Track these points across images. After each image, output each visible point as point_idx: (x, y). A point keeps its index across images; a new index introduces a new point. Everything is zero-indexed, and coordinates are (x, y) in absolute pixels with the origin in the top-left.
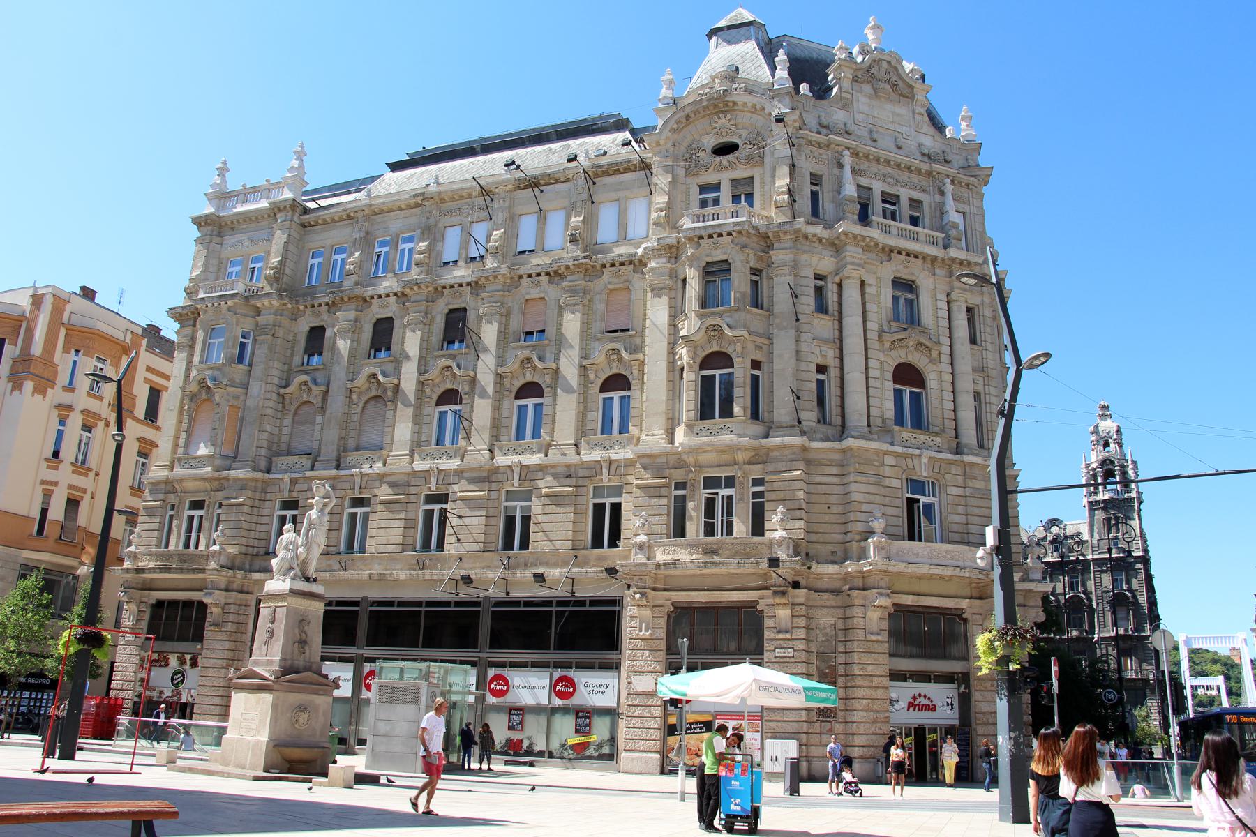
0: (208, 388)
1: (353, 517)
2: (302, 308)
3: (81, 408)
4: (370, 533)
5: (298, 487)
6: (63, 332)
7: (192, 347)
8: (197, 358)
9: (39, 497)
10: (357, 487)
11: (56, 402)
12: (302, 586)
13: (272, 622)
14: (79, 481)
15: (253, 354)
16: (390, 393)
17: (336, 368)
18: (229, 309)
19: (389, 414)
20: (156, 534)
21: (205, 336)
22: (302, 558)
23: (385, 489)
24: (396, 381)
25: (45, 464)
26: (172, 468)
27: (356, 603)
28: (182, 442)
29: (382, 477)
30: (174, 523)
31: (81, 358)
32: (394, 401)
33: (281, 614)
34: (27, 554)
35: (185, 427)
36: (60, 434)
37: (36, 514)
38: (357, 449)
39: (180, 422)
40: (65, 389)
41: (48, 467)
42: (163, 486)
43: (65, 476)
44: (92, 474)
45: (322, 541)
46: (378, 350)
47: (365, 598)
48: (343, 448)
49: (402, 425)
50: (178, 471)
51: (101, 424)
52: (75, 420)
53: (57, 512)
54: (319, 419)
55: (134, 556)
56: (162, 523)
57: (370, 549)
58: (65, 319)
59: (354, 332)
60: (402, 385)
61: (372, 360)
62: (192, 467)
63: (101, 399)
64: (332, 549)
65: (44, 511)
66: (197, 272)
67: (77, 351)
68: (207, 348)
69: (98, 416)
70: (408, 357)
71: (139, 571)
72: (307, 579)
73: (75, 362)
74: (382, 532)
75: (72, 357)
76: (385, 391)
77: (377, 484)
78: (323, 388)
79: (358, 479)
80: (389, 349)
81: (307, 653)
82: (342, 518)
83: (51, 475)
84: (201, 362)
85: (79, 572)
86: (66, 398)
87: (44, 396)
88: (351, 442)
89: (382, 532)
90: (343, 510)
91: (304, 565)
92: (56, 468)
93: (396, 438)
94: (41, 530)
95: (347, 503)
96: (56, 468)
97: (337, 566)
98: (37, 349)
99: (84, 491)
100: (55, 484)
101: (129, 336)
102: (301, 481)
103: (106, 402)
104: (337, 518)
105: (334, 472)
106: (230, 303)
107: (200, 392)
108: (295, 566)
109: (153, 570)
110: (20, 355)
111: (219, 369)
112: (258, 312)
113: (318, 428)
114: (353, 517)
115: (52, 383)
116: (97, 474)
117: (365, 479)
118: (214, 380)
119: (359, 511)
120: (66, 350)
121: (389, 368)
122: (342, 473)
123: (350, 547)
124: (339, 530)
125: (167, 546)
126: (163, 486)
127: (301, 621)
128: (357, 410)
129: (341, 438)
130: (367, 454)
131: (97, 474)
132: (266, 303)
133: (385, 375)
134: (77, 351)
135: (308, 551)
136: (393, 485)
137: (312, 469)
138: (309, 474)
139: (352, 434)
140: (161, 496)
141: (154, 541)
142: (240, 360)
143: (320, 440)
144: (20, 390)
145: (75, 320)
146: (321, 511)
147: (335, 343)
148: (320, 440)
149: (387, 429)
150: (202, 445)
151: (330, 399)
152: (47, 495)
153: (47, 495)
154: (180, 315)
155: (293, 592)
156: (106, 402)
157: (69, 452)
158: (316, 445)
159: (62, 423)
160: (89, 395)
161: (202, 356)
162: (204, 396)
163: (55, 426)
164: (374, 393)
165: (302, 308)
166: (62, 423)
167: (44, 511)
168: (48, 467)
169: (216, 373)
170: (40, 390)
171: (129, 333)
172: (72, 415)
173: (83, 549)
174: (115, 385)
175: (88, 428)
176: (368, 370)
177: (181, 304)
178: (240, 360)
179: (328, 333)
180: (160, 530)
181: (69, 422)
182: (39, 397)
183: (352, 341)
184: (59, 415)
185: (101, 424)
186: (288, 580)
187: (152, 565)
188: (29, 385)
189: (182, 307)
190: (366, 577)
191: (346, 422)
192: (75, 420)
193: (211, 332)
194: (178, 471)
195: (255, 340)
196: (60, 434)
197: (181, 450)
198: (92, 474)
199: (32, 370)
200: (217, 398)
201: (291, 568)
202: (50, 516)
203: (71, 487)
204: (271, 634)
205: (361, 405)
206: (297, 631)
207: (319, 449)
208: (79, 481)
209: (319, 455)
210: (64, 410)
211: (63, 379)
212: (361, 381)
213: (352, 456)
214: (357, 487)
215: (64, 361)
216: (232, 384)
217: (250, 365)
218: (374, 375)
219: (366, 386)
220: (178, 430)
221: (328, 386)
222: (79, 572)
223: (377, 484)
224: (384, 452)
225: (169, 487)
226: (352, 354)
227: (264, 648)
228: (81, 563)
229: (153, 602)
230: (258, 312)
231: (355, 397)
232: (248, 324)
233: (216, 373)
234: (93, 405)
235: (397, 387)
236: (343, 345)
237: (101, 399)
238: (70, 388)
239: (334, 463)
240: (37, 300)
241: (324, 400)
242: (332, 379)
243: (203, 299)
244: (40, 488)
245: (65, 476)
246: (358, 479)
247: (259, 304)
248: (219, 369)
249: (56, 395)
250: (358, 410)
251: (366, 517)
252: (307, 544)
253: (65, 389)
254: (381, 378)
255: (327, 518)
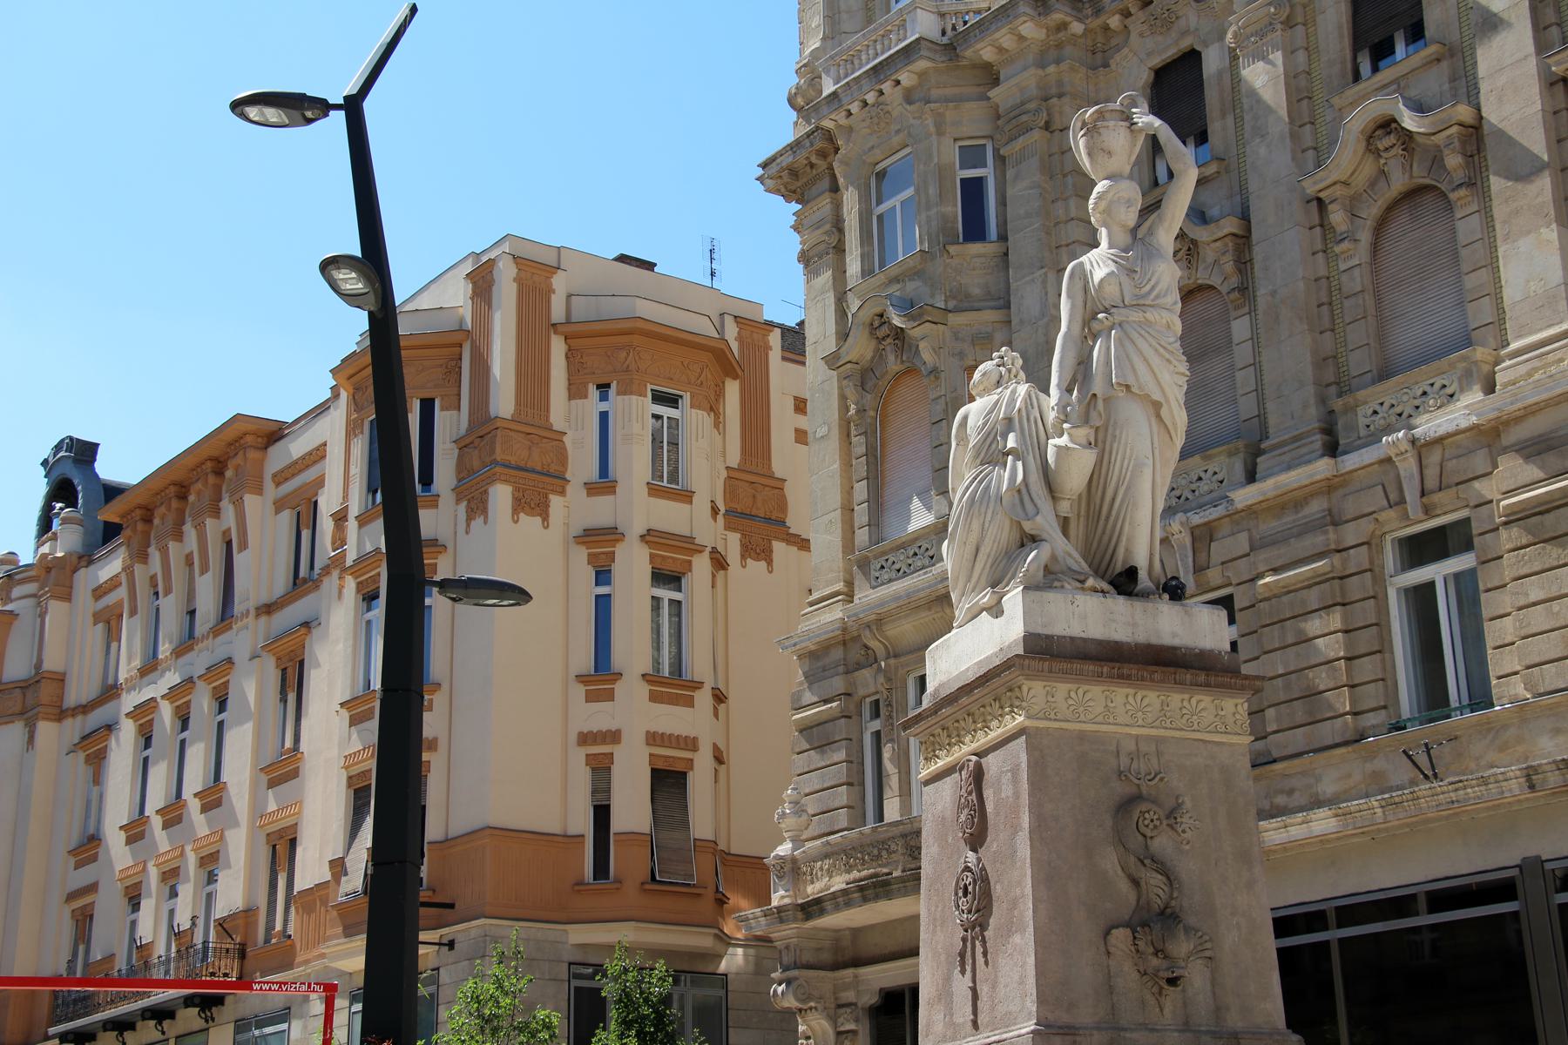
0: (899, 334)
1: (1422, 598)
2: (1115, 22)
3: (639, 528)
4: (1494, 632)
5: (1219, 550)
6: (558, 347)
7: (840, 249)
8: (853, 266)
9: (582, 778)
10: (1411, 494)
11: (577, 529)
12: (1091, 615)
13: (976, 840)
14: (672, 720)
15: (1002, 202)
16: (1453, 161)
17: (1259, 151)
18: (909, 98)
19: (1468, 227)
20: (842, 795)
21: (865, 199)
22: (1075, 479)
23: (1512, 469)
24: (1464, 112)
25: (580, 690)
26: (850, 596)
27: (1502, 889)
28: (861, 514)
29: (1489, 438)
30: (887, 753)
31: (617, 403)
32: (1475, 182)
33: (1008, 778)
34: (580, 935)
35: (860, 466)
36: (603, 606)
37: (582, 823)
38: (1384, 373)
39: (847, 464)
40: (592, 489)
41: (591, 697)
42: (837, 654)
43: (635, 713)
44: (704, 698)
45: (1169, 378)
46: (1382, 52)
47: (1532, 865)
48: (1335, 383)
49: (1524, 244)
50: (868, 596)
51: (701, 566)
52: (633, 564)
53: (633, 810)
54: (1240, 328)
55: (794, 870)
56: (855, 762)
57: (1509, 691)
58: (558, 312)
59: (1289, 24)
60: (1491, 114)
61: (1370, 82)
62: (901, 574)
63: (686, 496)
64: (1371, 720)
65: (602, 814)
66: (815, 44)
67: (603, 388)
68: (875, 231)
69: (688, 545)
70: (1491, 23)
71: (812, 909)
72: (1125, 582)
73: (604, 417)
74: (1538, 619)
75: (592, 404)
76: (1436, 160)
77: (1480, 462)
78: (1230, 225)
79: (1407, 467)
80: (1416, 33)
81: (1197, 977)
82: (1383, 610)
83: (599, 717)
84: (867, 272)
85: (723, 967)
86: (600, 511)
87: (545, 518)
88: (1359, 362)
89: (1538, 619)
90: (1380, 581)
91: (1095, 515)
92: (609, 696)
93: (1510, 294)
94: (601, 868)
95: (1390, 558)
96: (609, 696)
97: (1404, 772)
98: (503, 403)
99: (691, 744)
100: (614, 737)
101: (731, 331)
102: (1226, 527)
103: (701, 504)
104: (1367, 612)
105: (1323, 467)
106: (906, 78)
107: (879, 355)
108: (1045, 522)
109: (843, 899)
110: (470, 430)
111: (916, 274)
112: (991, 76)
113: (1243, 354)
114: (1422, 598)
115: (558, 480)
116: (719, 697)
117: (1434, 458)
118: (908, 306)
119: (1436, 572)
120: (575, 391)
121: (1433, 83)
122: (1351, 461)
123: (1434, 699)
124: (1383, 648)
125: (880, 816)
126: (837, 654)
127: (1126, 805)
128: (1355, 254)
129: (1321, 362)
130: (1420, 379)
131: (719, 697)
132: (1007, 41)
133: (1419, 108)
134: (603, 388)
135: (1101, 442)
136: (1534, 449)
137: (1251, 477)
138: (1245, 496)
139: (1357, 334)
140: (838, 684)
141: (842, 818)
142: (974, 229)
143: (1259, 391)
144: (485, 511)
145: (581, 309)
146: (1137, 239)
147: (1236, 80)
148: (1259, 391)
149: (1470, 281)
150: (916, 503)
151: (1258, 253)
152: (601, 770)
153: (601, 770)
154: (794, 173)
155: (1044, 652)
156: (701, 504)
157: (633, 647)
158: (1247, 407)
159: (603, 576)
160: (654, 491)
161: (866, 257)
162: (893, 364)
163: (586, 589)
164: (1399, 182)
165: (1115, 22)
166: (603, 576)
167: (602, 814)
168: (591, 697)
169: (912, 287)
170: (532, 503)
171: (729, 321)
172: (620, 551)
173: (721, 901)
174: (338, 119)
175: (666, 577)
176: (1358, 119)
177: (789, 137)
178: (974, 229)
179: (1212, 62)
180: (854, 782)
181: (618, 569)
182: (530, 523)
183: (1289, 53)
184: (592, 558)
185: (701, 566)
186: (1014, 598)
187: (839, 883)
188: (501, 495)
189: (794, 147)
190: (1515, 786)
191: (1326, 303)
192: (633, 564)
193: (878, 181)
194: (868, 596)
195: (1001, 160)
196: (603, 606)
197: (862, 536)
198: (704, 698)
199: (499, 456)
200: (927, 355)
201: (1028, 540)
202: (618, 823)
203: (653, 738)
204: (978, 896)
205: (1365, 237)
206: (1110, 861)
207: (1262, 417)
208: (672, 720)
209: (1265, 435)
210: (599, 542)
211: (583, 465)
212: (1346, 158)
213: (1372, 400)
214: (1411, 494)
215: (572, 417)
216: (963, 302)
217: (1003, 237)
218: (1388, 125)
219: (1368, 169)
220: (848, 491)
221: (1245, 217)
222: (723, 967)
223: (1480, 462)
224: (1480, 353)
225: (856, 654)
226: (1299, 90)
227: (962, 984)
228: (726, 941)
229: (871, 999)
230: (991, 76)
231: (1337, 217)
232: (971, 120)
233: (912, 287)
234: (670, 516)
235: (1475, 134)
236: (1263, 77)
237: (686, 496)
238: (604, 483)
239: (1318, 441)
240: (482, 279)
241: (1243, 263)
242: (1253, 185)
243: (834, 94)
244: (579, 755)
245: (635, 713)
246: (1407, 467)
247: (988, 54)
248: (916, 274)
249: (573, 508)
250: (1361, 253)
251: (1467, 589)
252: (1094, 409)
253: (592, 489)
254: (1410, 121)
255: (1167, 275)
